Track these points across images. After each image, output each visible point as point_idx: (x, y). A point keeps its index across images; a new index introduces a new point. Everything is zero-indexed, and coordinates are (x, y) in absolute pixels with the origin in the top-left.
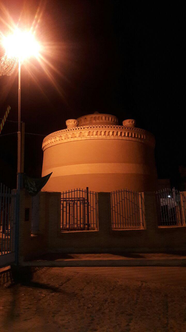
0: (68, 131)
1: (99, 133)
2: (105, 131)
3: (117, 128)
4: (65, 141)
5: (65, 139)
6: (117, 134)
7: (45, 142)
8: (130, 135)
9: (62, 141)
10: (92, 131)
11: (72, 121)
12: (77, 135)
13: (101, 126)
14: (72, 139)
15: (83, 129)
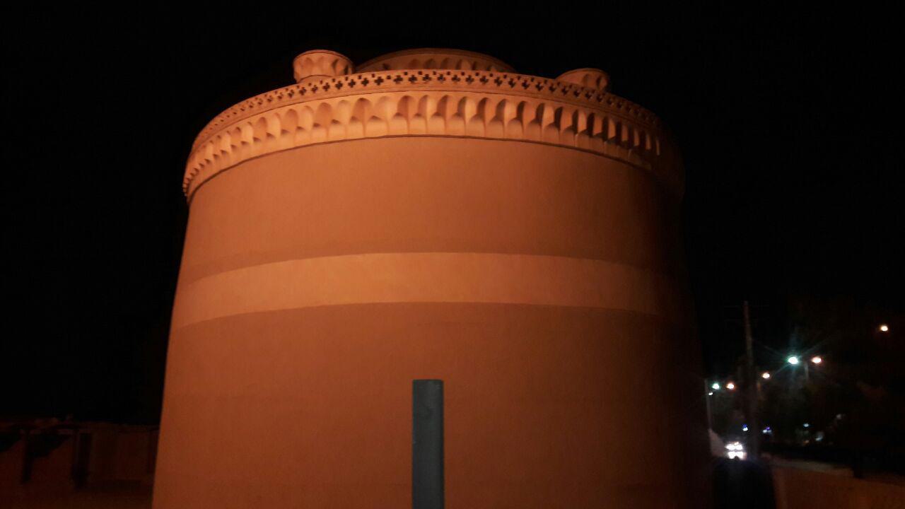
0: (297, 96)
1: (451, 108)
2: (480, 97)
3: (539, 88)
4: (285, 143)
5: (316, 125)
6: (538, 119)
7: (205, 147)
8: (598, 129)
9: (271, 146)
10: (494, 100)
11: (322, 58)
12: (345, 114)
13: (435, 73)
14: (320, 136)
15: (372, 84)
